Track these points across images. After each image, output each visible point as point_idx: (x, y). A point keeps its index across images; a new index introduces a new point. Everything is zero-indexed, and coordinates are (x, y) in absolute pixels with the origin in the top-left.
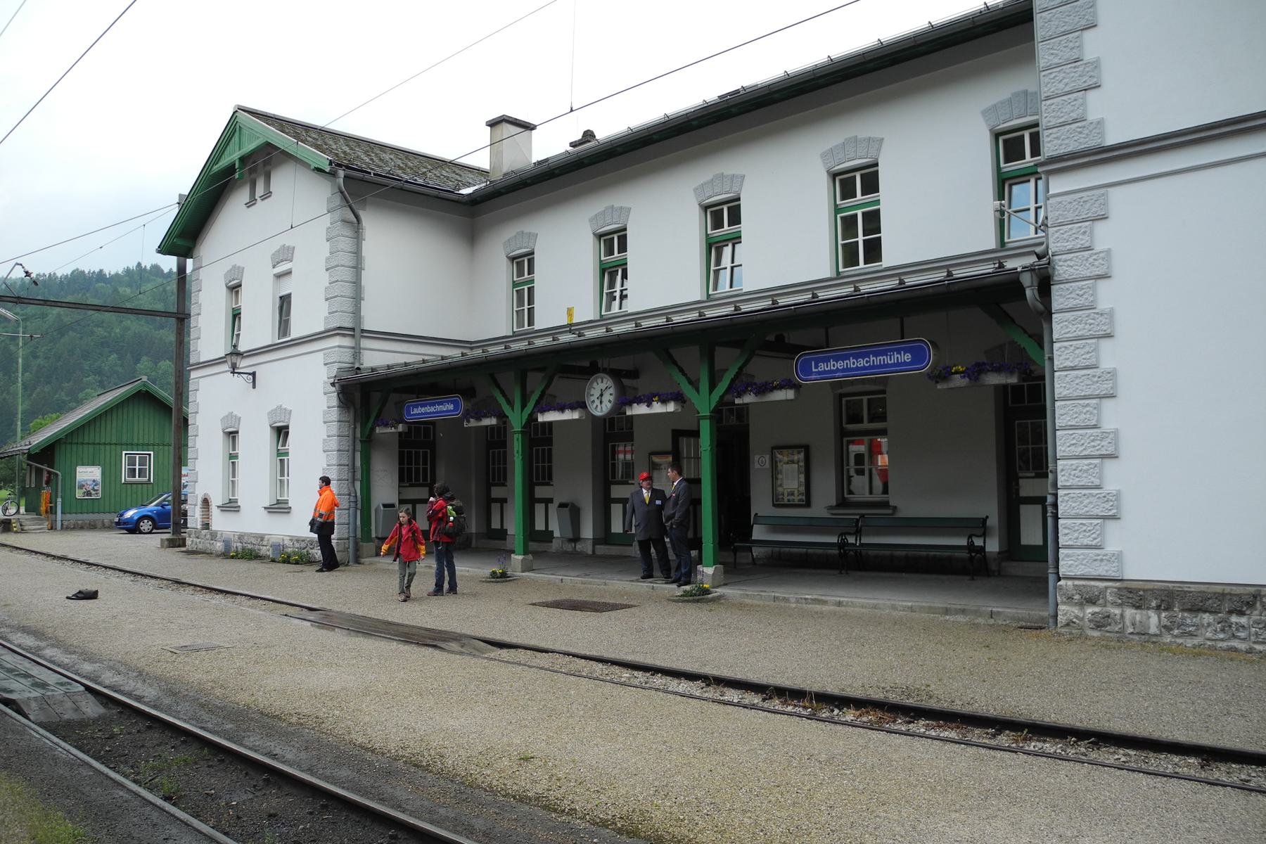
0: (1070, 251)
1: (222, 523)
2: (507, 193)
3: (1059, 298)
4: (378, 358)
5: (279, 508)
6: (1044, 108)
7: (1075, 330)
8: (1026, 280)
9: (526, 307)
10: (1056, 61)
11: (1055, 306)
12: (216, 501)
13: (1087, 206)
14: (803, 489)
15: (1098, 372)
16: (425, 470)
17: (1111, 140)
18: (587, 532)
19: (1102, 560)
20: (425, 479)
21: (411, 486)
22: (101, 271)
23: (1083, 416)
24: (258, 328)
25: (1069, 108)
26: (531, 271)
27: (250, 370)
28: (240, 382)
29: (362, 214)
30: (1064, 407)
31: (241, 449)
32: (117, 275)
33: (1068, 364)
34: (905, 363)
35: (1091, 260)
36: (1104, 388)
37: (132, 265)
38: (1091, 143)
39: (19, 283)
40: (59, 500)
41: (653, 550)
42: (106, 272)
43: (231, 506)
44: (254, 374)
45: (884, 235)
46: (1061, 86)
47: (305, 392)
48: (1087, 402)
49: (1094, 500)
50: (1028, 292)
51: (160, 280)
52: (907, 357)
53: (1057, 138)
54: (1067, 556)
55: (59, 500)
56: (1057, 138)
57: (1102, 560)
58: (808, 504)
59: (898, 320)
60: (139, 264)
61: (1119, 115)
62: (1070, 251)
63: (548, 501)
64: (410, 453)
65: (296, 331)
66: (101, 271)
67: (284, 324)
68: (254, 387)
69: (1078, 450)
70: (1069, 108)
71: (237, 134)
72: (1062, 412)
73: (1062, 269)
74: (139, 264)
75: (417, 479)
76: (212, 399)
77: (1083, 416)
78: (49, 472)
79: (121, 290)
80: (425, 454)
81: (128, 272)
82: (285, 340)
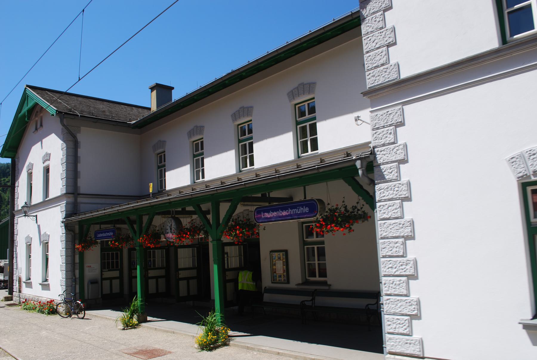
0: (384, 145)
1: (26, 292)
2: (161, 117)
6: (365, 59)
7: (390, 194)
8: (358, 164)
9: (309, 138)
10: (370, 30)
12: (24, 279)
13: (391, 116)
14: (285, 274)
15: (402, 221)
16: (117, 262)
17: (404, 75)
19: (410, 344)
20: (117, 266)
21: (109, 271)
23: (395, 250)
25: (378, 58)
26: (202, 149)
27: (35, 214)
29: (80, 137)
30: (384, 243)
33: (385, 216)
34: (306, 213)
35: (395, 150)
36: (407, 231)
38: (393, 76)
39: (6, 166)
46: (374, 44)
48: (397, 240)
49: (404, 303)
50: (360, 172)
53: (373, 76)
54: (390, 339)
56: (373, 76)
57: (410, 344)
58: (288, 282)
59: (302, 188)
61: (410, 60)
62: (384, 145)
64: (108, 254)
65: (52, 195)
69: (393, 271)
70: (378, 58)
71: (26, 102)
72: (383, 246)
73: (381, 158)
75: (113, 267)
77: (395, 250)
80: (117, 254)
82: (47, 203)
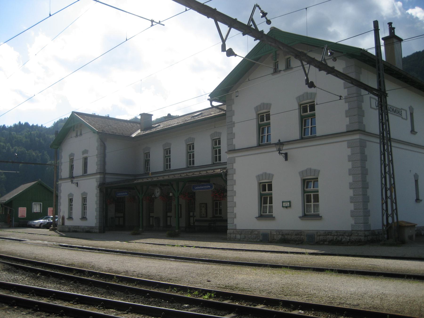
1: (68, 223)
3: (228, 178)
4: (109, 179)
5: (84, 218)
11: (228, 179)
18: (161, 224)
22: (4, 125)
24: (78, 170)
27: (76, 182)
28: (74, 186)
31: (74, 203)
32: (11, 127)
37: (17, 123)
38: (233, 149)
40: (14, 218)
41: (33, 183)
42: (6, 126)
43: (70, 218)
44: (77, 183)
45: (221, 155)
47: (91, 187)
51: (28, 129)
52: (209, 187)
55: (14, 218)
58: (207, 216)
60: (20, 122)
63: (153, 217)
65: (89, 172)
66: (4, 125)
67: (85, 170)
68: (77, 186)
74: (20, 122)
76: (66, 189)
78: (10, 209)
79: (12, 133)
81: (15, 126)
